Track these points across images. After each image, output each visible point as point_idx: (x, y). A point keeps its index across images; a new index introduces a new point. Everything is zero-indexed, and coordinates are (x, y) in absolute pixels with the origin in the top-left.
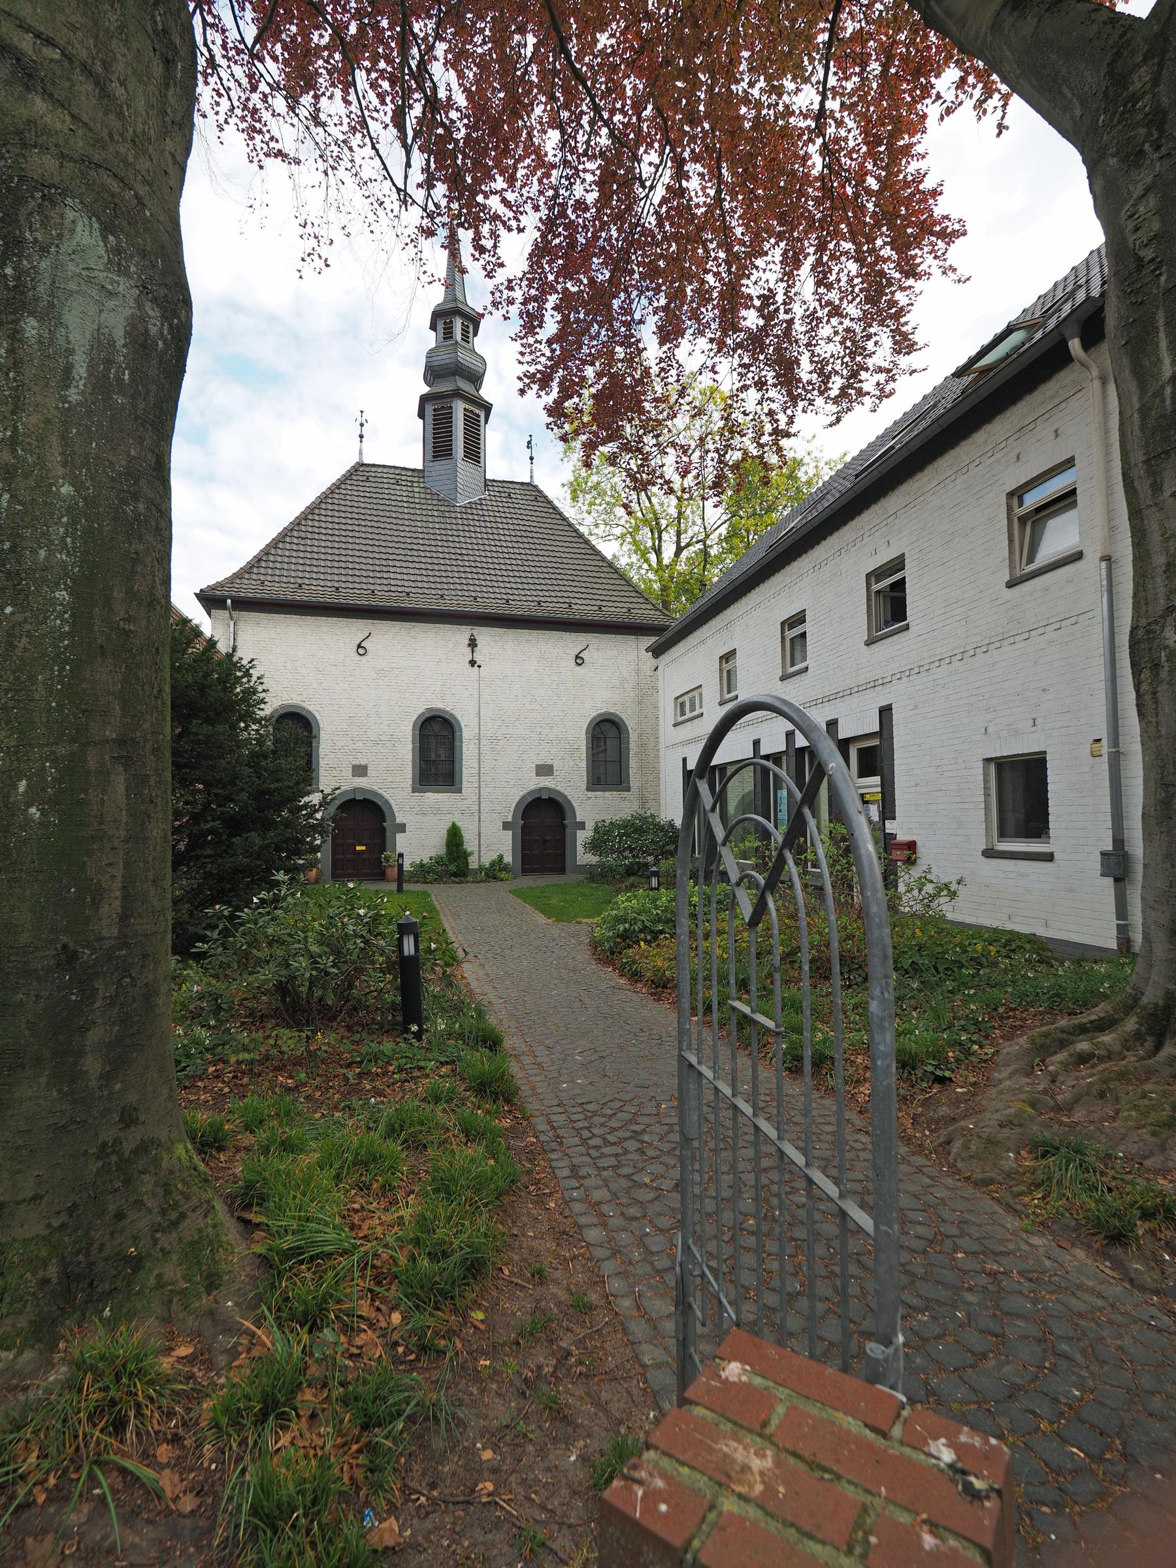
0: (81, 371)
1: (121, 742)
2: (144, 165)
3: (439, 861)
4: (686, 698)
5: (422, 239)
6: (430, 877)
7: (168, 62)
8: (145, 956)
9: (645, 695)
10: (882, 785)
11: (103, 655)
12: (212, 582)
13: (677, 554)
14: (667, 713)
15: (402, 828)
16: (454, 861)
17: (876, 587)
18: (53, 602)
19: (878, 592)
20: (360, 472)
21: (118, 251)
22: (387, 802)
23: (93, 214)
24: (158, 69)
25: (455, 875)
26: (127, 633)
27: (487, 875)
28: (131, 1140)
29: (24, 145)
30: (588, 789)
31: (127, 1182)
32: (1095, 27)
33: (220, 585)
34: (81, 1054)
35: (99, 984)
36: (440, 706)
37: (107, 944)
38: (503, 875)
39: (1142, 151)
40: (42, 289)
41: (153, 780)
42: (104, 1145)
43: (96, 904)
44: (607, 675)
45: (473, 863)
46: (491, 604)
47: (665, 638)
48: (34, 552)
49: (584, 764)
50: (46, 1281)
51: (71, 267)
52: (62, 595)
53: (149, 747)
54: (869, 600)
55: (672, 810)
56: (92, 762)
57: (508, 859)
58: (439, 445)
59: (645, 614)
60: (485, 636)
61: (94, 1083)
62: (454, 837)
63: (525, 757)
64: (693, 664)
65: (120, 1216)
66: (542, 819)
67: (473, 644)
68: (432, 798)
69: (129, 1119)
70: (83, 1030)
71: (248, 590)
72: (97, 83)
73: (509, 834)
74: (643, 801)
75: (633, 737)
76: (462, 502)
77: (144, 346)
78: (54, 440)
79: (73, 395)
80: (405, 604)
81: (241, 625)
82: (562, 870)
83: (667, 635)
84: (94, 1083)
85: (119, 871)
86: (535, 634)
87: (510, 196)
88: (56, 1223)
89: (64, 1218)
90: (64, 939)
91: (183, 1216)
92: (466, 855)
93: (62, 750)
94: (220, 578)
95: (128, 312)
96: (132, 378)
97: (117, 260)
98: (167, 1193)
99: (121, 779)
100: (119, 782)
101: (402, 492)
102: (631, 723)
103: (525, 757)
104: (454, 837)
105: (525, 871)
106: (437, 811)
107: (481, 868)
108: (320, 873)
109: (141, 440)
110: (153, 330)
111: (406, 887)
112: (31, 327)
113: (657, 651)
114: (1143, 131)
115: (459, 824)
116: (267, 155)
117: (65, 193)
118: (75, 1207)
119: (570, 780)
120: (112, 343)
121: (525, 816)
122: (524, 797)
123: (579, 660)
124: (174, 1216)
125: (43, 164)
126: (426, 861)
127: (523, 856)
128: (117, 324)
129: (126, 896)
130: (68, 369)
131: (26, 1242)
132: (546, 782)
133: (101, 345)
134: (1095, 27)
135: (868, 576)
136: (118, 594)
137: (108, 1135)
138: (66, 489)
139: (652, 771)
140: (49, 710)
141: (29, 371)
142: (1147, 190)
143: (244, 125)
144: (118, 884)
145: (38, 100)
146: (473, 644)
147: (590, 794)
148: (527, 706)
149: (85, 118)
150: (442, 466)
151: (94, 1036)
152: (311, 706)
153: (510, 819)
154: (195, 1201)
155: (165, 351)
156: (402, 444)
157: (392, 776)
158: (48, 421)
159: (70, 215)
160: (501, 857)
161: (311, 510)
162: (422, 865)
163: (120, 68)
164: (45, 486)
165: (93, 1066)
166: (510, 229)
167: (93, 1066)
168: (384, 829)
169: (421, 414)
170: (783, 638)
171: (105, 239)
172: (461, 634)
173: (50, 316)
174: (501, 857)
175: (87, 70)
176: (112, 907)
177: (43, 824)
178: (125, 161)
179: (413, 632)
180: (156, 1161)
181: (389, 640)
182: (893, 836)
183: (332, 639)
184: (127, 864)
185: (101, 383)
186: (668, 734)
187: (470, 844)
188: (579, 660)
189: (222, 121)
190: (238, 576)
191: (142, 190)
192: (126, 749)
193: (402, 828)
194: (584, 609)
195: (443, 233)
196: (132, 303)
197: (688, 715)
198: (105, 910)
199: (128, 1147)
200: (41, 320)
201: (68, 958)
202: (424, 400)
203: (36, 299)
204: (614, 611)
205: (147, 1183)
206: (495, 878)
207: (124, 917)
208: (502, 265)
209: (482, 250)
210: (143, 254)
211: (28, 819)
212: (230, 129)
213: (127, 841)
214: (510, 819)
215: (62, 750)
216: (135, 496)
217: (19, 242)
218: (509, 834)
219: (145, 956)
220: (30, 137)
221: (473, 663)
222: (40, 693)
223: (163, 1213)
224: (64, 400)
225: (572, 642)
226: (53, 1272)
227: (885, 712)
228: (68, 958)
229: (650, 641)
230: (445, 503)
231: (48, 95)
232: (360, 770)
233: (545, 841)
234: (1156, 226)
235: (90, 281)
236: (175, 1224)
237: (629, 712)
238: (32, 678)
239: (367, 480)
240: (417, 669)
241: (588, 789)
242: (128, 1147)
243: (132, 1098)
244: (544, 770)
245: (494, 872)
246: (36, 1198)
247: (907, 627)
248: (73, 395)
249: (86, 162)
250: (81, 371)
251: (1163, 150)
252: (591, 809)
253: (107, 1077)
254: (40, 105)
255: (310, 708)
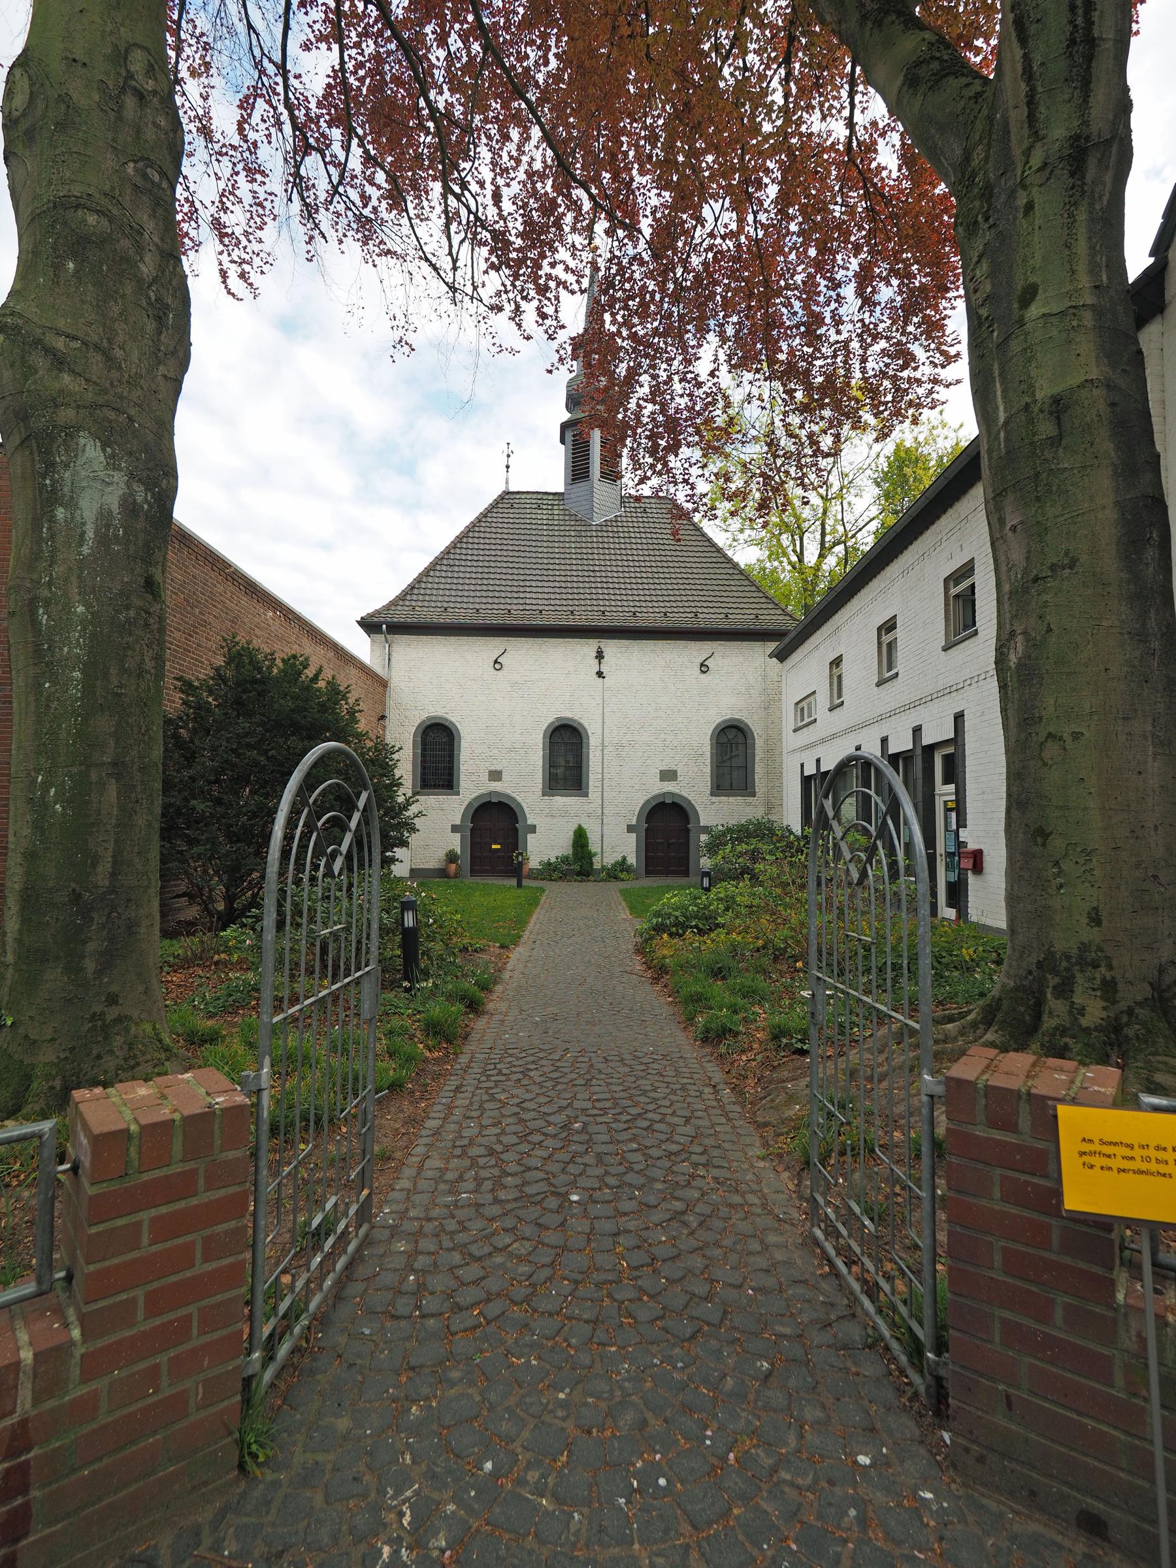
0: (90, 534)
1: (115, 764)
2: (136, 394)
3: (565, 860)
4: (804, 704)
5: (492, 315)
6: (555, 875)
7: (160, 319)
8: (129, 900)
9: (770, 702)
10: (957, 793)
11: (102, 710)
12: (371, 610)
13: (822, 556)
14: (789, 719)
15: (533, 829)
16: (579, 862)
17: (954, 591)
18: (72, 679)
19: (957, 596)
20: (507, 498)
21: (113, 456)
22: (519, 805)
23: (96, 437)
24: (151, 326)
25: (579, 874)
26: (119, 695)
27: (609, 875)
28: (112, 1013)
29: (56, 406)
30: (712, 794)
31: (106, 1038)
32: (963, 102)
33: (378, 612)
34: (82, 957)
35: (95, 915)
36: (569, 715)
37: (101, 891)
38: (623, 875)
39: (976, 222)
40: (66, 489)
41: (139, 788)
42: (95, 1014)
43: (94, 865)
44: (733, 681)
45: (597, 865)
46: (617, 617)
47: (787, 643)
48: (61, 649)
49: (708, 770)
50: (53, 1088)
51: (84, 473)
52: (77, 674)
53: (135, 767)
54: (947, 604)
55: (792, 818)
56: (94, 777)
57: (632, 860)
58: (578, 471)
59: (771, 619)
60: (611, 647)
61: (90, 976)
62: (580, 838)
63: (649, 762)
64: (807, 671)
65: (99, 1057)
66: (666, 823)
67: (600, 656)
68: (563, 802)
69: (112, 1000)
70: (84, 942)
71: (400, 616)
72: (104, 354)
73: (633, 836)
74: (770, 807)
75: (759, 743)
76: (598, 520)
77: (133, 511)
78: (74, 580)
79: (86, 550)
80: (538, 622)
81: (395, 648)
82: (686, 873)
83: (787, 640)
84: (90, 976)
85: (111, 846)
86: (661, 645)
87: (572, 264)
88: (62, 1056)
89: (67, 1054)
90: (73, 885)
91: (138, 1064)
92: (590, 856)
93: (75, 770)
94: (378, 605)
95: (121, 492)
96: (125, 533)
97: (112, 463)
98: (130, 1049)
99: (114, 787)
100: (112, 790)
101: (542, 515)
102: (757, 729)
103: (649, 762)
104: (580, 838)
105: (649, 873)
106: (565, 814)
107: (603, 868)
108: (459, 867)
109: (133, 570)
110: (139, 499)
111: (525, 882)
112: (60, 513)
113: (782, 656)
114: (977, 203)
115: (585, 826)
116: (379, 255)
117: (78, 430)
118: (73, 1048)
119: (694, 785)
120: (110, 513)
121: (649, 819)
122: (648, 802)
123: (704, 668)
124: (132, 1062)
125: (67, 415)
126: (553, 860)
127: (647, 858)
128: (113, 501)
129: (115, 862)
130: (83, 534)
131: (46, 1064)
132: (670, 787)
133: (104, 516)
134: (963, 102)
135: (946, 581)
136: (113, 671)
137: (97, 1008)
138: (80, 609)
139: (775, 774)
140: (68, 745)
141: (60, 539)
142: (981, 257)
143: (360, 235)
144: (110, 853)
145: (66, 376)
146: (600, 656)
147: (714, 799)
148: (652, 715)
149: (95, 379)
150: (581, 487)
151: (91, 947)
152: (454, 718)
153: (458, 822)
154: (148, 1057)
155: (149, 510)
156: (546, 470)
157: (524, 782)
158: (70, 569)
159: (82, 441)
160: (624, 858)
161: (460, 539)
162: (549, 864)
163: (120, 339)
164: (68, 608)
165: (90, 965)
166: (573, 292)
167: (90, 965)
168: (516, 830)
169: (563, 441)
170: (880, 643)
171: (104, 451)
172: (586, 648)
173: (71, 504)
174: (624, 858)
175: (97, 347)
176: (105, 867)
177: (63, 815)
178: (121, 397)
179: (544, 647)
180: (127, 1030)
181: (523, 655)
182: (964, 844)
183: (474, 655)
184: (116, 841)
185: (103, 540)
186: (790, 740)
187: (594, 847)
188: (704, 668)
189: (340, 234)
190: (394, 603)
191: (132, 412)
192: (118, 769)
193: (533, 829)
194: (710, 618)
195: (509, 308)
196: (123, 485)
197: (807, 720)
198: (100, 869)
199: (109, 1018)
200: (66, 508)
201: (76, 897)
202: (564, 427)
203: (64, 496)
204: (741, 619)
205: (118, 1041)
206: (616, 878)
207: (113, 875)
208: (563, 327)
209: (544, 316)
210: (131, 454)
211: (55, 812)
212: (349, 241)
213: (117, 826)
214: (458, 822)
215: (75, 770)
216: (128, 607)
217: (53, 464)
218: (633, 836)
219: (129, 900)
220: (60, 400)
221: (600, 674)
222: (63, 735)
223: (126, 1060)
224: (80, 553)
225: (696, 651)
226: (58, 1083)
227: (959, 718)
228: (76, 897)
229: (772, 646)
230: (582, 523)
231: (72, 372)
232: (496, 775)
233: (669, 845)
234: (988, 288)
235: (95, 479)
236: (133, 1067)
237: (755, 718)
238: (59, 725)
239: (512, 507)
240: (550, 680)
241: (712, 794)
242: (109, 1018)
243: (114, 988)
244: (668, 775)
245: (619, 871)
246: (53, 1040)
247: (976, 633)
248: (86, 550)
249: (96, 406)
250: (90, 534)
251: (991, 221)
252: (714, 813)
253: (99, 973)
254: (66, 378)
255: (453, 719)
